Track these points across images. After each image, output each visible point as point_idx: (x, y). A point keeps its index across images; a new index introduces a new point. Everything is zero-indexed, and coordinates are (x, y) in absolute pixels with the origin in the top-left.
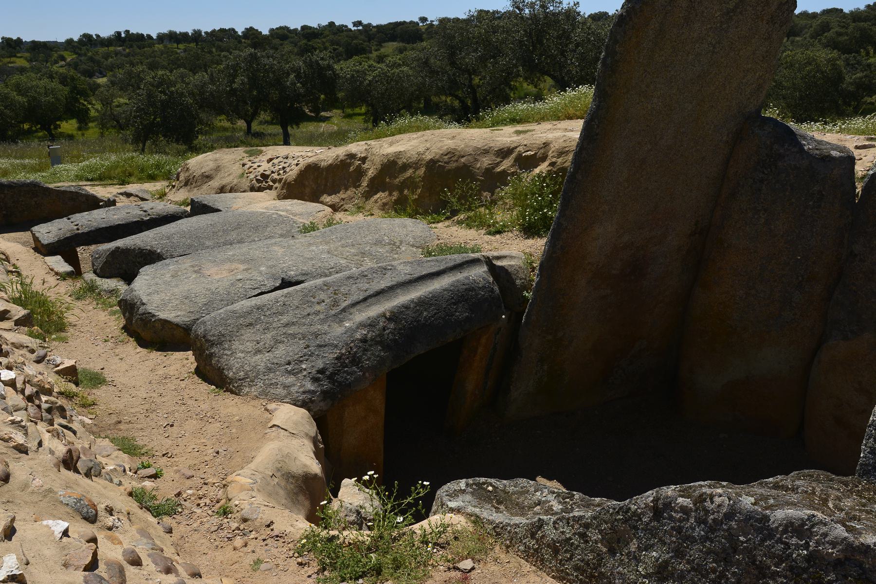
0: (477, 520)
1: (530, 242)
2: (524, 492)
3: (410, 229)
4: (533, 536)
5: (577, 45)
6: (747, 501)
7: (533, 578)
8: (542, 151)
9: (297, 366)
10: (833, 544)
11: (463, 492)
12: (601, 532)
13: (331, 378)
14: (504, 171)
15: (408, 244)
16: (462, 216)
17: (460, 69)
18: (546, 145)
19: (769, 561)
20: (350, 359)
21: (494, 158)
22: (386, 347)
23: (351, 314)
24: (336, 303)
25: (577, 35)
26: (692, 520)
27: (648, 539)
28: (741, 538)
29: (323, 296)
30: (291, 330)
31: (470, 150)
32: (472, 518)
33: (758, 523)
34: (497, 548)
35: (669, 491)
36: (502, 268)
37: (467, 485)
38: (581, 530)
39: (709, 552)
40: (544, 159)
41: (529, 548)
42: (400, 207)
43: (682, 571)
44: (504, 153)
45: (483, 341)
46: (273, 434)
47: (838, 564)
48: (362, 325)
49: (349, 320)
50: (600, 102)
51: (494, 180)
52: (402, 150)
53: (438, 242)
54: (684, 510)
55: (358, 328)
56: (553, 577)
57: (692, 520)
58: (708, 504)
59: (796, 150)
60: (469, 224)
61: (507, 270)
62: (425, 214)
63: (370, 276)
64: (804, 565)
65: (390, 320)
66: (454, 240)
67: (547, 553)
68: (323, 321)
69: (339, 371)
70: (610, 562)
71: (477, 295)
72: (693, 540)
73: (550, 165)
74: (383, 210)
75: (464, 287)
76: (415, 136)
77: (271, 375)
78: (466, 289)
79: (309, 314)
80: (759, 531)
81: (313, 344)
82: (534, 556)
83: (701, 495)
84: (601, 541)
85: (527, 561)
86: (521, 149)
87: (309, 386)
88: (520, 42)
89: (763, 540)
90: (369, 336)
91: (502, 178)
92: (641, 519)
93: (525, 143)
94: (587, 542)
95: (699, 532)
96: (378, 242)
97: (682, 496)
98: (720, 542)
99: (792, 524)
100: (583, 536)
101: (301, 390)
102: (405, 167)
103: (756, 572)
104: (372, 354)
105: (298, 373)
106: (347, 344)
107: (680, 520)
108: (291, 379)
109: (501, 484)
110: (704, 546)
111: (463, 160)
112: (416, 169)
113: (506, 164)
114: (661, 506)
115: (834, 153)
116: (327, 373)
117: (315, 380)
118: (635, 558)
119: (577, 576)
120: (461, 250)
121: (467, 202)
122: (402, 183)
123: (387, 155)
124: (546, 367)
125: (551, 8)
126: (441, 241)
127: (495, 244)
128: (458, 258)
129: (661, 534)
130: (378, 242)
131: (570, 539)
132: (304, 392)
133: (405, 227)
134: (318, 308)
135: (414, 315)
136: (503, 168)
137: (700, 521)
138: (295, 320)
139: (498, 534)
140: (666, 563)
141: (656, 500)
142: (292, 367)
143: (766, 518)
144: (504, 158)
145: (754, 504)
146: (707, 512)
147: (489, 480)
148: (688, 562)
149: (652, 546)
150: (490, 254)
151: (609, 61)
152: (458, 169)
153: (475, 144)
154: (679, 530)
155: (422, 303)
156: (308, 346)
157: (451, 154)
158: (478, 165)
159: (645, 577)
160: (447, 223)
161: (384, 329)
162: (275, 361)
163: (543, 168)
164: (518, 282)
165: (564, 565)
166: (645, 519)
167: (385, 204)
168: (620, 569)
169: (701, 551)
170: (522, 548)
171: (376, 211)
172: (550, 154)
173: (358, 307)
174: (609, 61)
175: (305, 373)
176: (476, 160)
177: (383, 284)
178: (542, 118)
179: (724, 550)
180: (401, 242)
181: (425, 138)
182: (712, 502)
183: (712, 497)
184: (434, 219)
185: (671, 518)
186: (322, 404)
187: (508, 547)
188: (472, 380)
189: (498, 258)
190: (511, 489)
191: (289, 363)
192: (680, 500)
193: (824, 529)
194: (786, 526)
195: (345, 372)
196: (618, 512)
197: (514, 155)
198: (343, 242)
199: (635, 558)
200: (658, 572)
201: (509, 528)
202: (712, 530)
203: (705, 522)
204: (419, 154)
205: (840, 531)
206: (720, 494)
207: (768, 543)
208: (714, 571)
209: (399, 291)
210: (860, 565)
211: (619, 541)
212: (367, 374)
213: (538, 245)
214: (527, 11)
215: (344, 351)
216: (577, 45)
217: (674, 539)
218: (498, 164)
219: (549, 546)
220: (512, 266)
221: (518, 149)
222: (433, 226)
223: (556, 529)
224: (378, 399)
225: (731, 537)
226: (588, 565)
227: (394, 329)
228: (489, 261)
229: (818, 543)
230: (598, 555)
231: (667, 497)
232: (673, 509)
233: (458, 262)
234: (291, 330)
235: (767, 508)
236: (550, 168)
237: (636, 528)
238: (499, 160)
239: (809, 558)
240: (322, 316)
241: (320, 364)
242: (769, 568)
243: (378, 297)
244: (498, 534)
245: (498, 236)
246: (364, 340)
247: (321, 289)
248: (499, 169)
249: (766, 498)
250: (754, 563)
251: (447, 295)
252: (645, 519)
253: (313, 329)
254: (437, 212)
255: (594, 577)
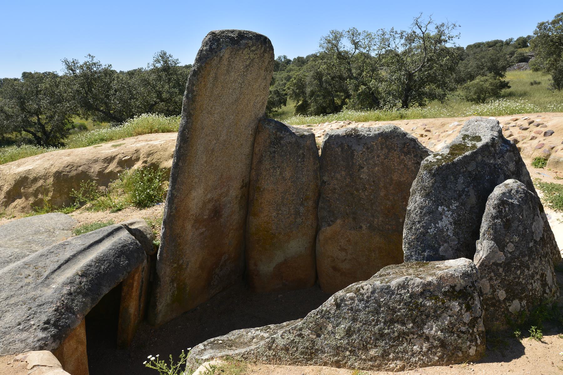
0: (227, 358)
1: (144, 211)
2: (241, 336)
3: (57, 219)
4: (270, 348)
5: (116, 91)
6: (378, 283)
7: (279, 370)
8: (135, 155)
9: (26, 324)
10: (418, 286)
11: (205, 349)
12: (309, 329)
13: (55, 325)
14: (111, 172)
15: (60, 229)
16: (88, 205)
17: (29, 112)
18: (137, 151)
19: (396, 305)
20: (65, 309)
21: (102, 164)
22: (85, 295)
23: (53, 279)
24: (39, 275)
25: (115, 85)
26: (356, 302)
27: (337, 320)
28: (381, 300)
29: (27, 272)
30: (12, 301)
31: (84, 161)
32: (225, 358)
33: (387, 291)
34: (249, 366)
35: (340, 293)
36: (136, 230)
37: (204, 345)
38: (298, 333)
39: (369, 312)
40: (138, 159)
41: (270, 356)
42: (37, 207)
43: (358, 328)
44: (109, 160)
45: (136, 278)
46: (37, 372)
47: (422, 294)
48: (65, 284)
49: (54, 283)
50: (187, 119)
51: (106, 178)
52: (31, 168)
53: (80, 224)
54: (352, 299)
55: (63, 286)
56: (290, 364)
57: (356, 302)
58: (362, 291)
59: (288, 134)
60: (98, 208)
61: (140, 230)
62: (60, 208)
63: (56, 252)
64: (410, 300)
65: (82, 276)
66: (91, 221)
67: (282, 354)
68: (35, 288)
69: (59, 318)
70: (319, 341)
71: (129, 248)
72: (360, 311)
73: (143, 163)
74: (23, 212)
75: (120, 245)
76: (37, 158)
77: (8, 336)
78: (122, 246)
79: (22, 287)
80: (388, 293)
81: (34, 305)
82: (275, 359)
83: (357, 289)
84: (312, 334)
85: (270, 364)
86: (120, 156)
87: (41, 335)
88: (77, 91)
89: (390, 297)
90: (72, 290)
91: (112, 176)
92: (330, 313)
93: (122, 152)
94: (303, 337)
95: (361, 306)
96: (37, 232)
97: (348, 293)
98: (372, 306)
99: (400, 284)
100: (300, 335)
101: (36, 339)
102: (35, 180)
103: (391, 313)
104: (78, 301)
105: (29, 329)
106: (59, 299)
107: (351, 304)
108: (25, 335)
109: (225, 337)
110: (366, 311)
111: (80, 168)
112: (45, 179)
113: (112, 167)
114: (339, 302)
115: (306, 133)
116: (52, 322)
117: (44, 329)
118: (333, 333)
119: (303, 357)
120: (100, 225)
121: (90, 195)
122: (36, 191)
123: (19, 173)
124: (175, 285)
125: (95, 69)
126: (82, 223)
127: (121, 217)
128: (109, 229)
129: (343, 315)
130: (37, 232)
131: (294, 340)
132: (39, 340)
133: (52, 218)
134: (27, 281)
135: (96, 270)
136: (110, 169)
137: (360, 301)
138: (12, 293)
139: (245, 359)
140: (350, 327)
141: (336, 300)
142: (23, 325)
143: (389, 287)
144: (109, 163)
145: (381, 283)
146: (362, 295)
147: (216, 338)
148: (360, 322)
149: (340, 323)
150: (127, 222)
151: (190, 96)
152: (78, 175)
153: (87, 157)
154: (351, 309)
155: (99, 261)
156: (31, 308)
157: (71, 165)
158: (92, 171)
159: (340, 340)
160: (78, 211)
161: (80, 283)
162: (7, 326)
163: (138, 165)
164: (148, 236)
165: (294, 355)
166: (332, 312)
167: (23, 208)
168: (326, 342)
169: (365, 314)
170: (265, 358)
171: (16, 214)
172: (141, 156)
173: (56, 273)
174: (190, 96)
175: (34, 327)
176: (90, 167)
177: (68, 255)
178: (123, 136)
179: (375, 309)
180: (54, 229)
181: (47, 158)
182: (364, 290)
183: (362, 287)
184: (68, 210)
185: (346, 305)
186: (53, 345)
187: (255, 362)
188: (133, 306)
189: (132, 224)
190: (232, 338)
191: (19, 324)
192: (348, 295)
193: (412, 282)
194: (398, 286)
195: (63, 318)
196: (317, 314)
197: (116, 161)
198: (8, 237)
199: (333, 333)
200: (347, 334)
201: (252, 352)
202: (367, 302)
203: (363, 300)
204: (45, 169)
205: (418, 280)
206: (366, 286)
207: (393, 297)
208: (373, 320)
209: (79, 257)
210: (429, 291)
211: (321, 329)
212: (78, 316)
213: (159, 210)
214: (78, 71)
215: (59, 304)
216: (116, 91)
217: (350, 314)
218: (106, 168)
219: (282, 349)
220: (142, 227)
221: (118, 156)
222: (70, 214)
223: (283, 339)
224: (81, 332)
225: (377, 302)
226: (307, 348)
227: (87, 281)
228: (127, 227)
229: (412, 288)
230: (312, 341)
231: (341, 296)
232: (345, 300)
233: (110, 231)
234: (12, 301)
235: (387, 283)
236: (144, 165)
237: (329, 318)
238: (106, 165)
239: (410, 297)
240: (33, 285)
241: (44, 318)
242: (396, 308)
243: (67, 264)
244: (245, 359)
245: (120, 212)
246: (70, 294)
247: (23, 268)
248: (107, 171)
249: (384, 279)
250: (389, 308)
251: (112, 252)
252: (332, 312)
253: (29, 296)
254: (68, 205)
255: (313, 353)
